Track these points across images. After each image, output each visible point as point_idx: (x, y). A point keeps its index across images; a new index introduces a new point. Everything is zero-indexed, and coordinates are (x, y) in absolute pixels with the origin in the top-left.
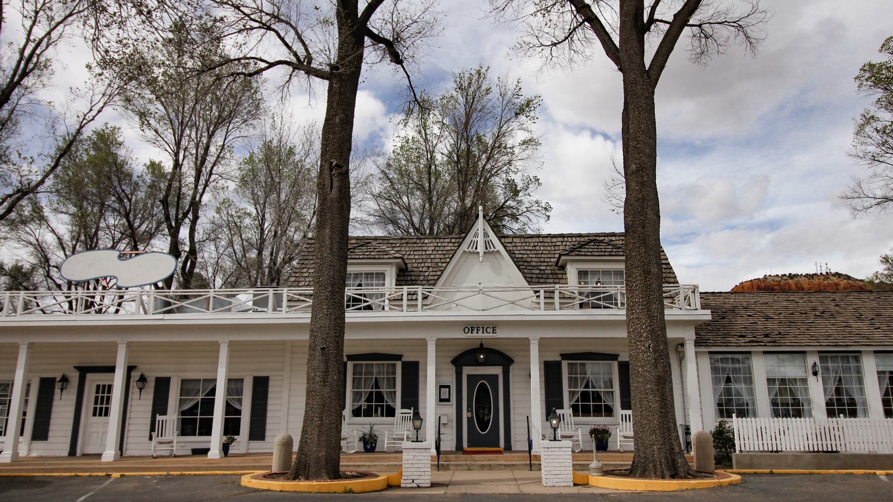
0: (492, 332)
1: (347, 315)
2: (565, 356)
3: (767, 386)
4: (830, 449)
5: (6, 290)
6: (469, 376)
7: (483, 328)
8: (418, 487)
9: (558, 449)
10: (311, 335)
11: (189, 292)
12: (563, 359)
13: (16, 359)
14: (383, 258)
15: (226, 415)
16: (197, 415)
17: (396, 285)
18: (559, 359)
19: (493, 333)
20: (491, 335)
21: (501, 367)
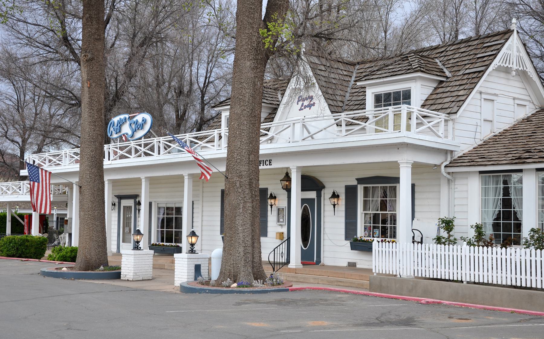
0: (269, 164)
1: (261, 147)
2: (361, 181)
3: (397, 212)
4: (519, 284)
5: (32, 154)
6: (124, 206)
7: (263, 161)
8: (128, 280)
9: (181, 259)
10: (227, 168)
11: (127, 144)
12: (358, 184)
13: (184, 182)
14: (372, 79)
15: (521, 223)
16: (513, 221)
17: (376, 107)
18: (355, 183)
19: (270, 165)
20: (269, 167)
21: (315, 192)
